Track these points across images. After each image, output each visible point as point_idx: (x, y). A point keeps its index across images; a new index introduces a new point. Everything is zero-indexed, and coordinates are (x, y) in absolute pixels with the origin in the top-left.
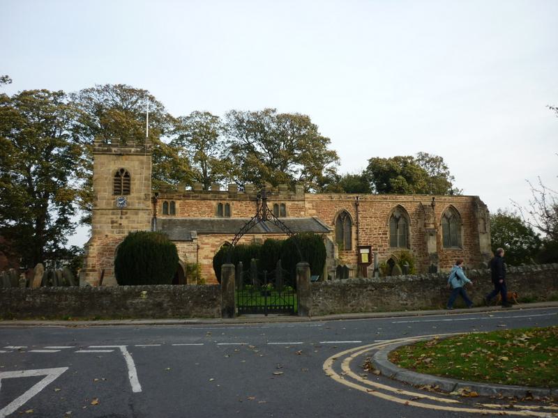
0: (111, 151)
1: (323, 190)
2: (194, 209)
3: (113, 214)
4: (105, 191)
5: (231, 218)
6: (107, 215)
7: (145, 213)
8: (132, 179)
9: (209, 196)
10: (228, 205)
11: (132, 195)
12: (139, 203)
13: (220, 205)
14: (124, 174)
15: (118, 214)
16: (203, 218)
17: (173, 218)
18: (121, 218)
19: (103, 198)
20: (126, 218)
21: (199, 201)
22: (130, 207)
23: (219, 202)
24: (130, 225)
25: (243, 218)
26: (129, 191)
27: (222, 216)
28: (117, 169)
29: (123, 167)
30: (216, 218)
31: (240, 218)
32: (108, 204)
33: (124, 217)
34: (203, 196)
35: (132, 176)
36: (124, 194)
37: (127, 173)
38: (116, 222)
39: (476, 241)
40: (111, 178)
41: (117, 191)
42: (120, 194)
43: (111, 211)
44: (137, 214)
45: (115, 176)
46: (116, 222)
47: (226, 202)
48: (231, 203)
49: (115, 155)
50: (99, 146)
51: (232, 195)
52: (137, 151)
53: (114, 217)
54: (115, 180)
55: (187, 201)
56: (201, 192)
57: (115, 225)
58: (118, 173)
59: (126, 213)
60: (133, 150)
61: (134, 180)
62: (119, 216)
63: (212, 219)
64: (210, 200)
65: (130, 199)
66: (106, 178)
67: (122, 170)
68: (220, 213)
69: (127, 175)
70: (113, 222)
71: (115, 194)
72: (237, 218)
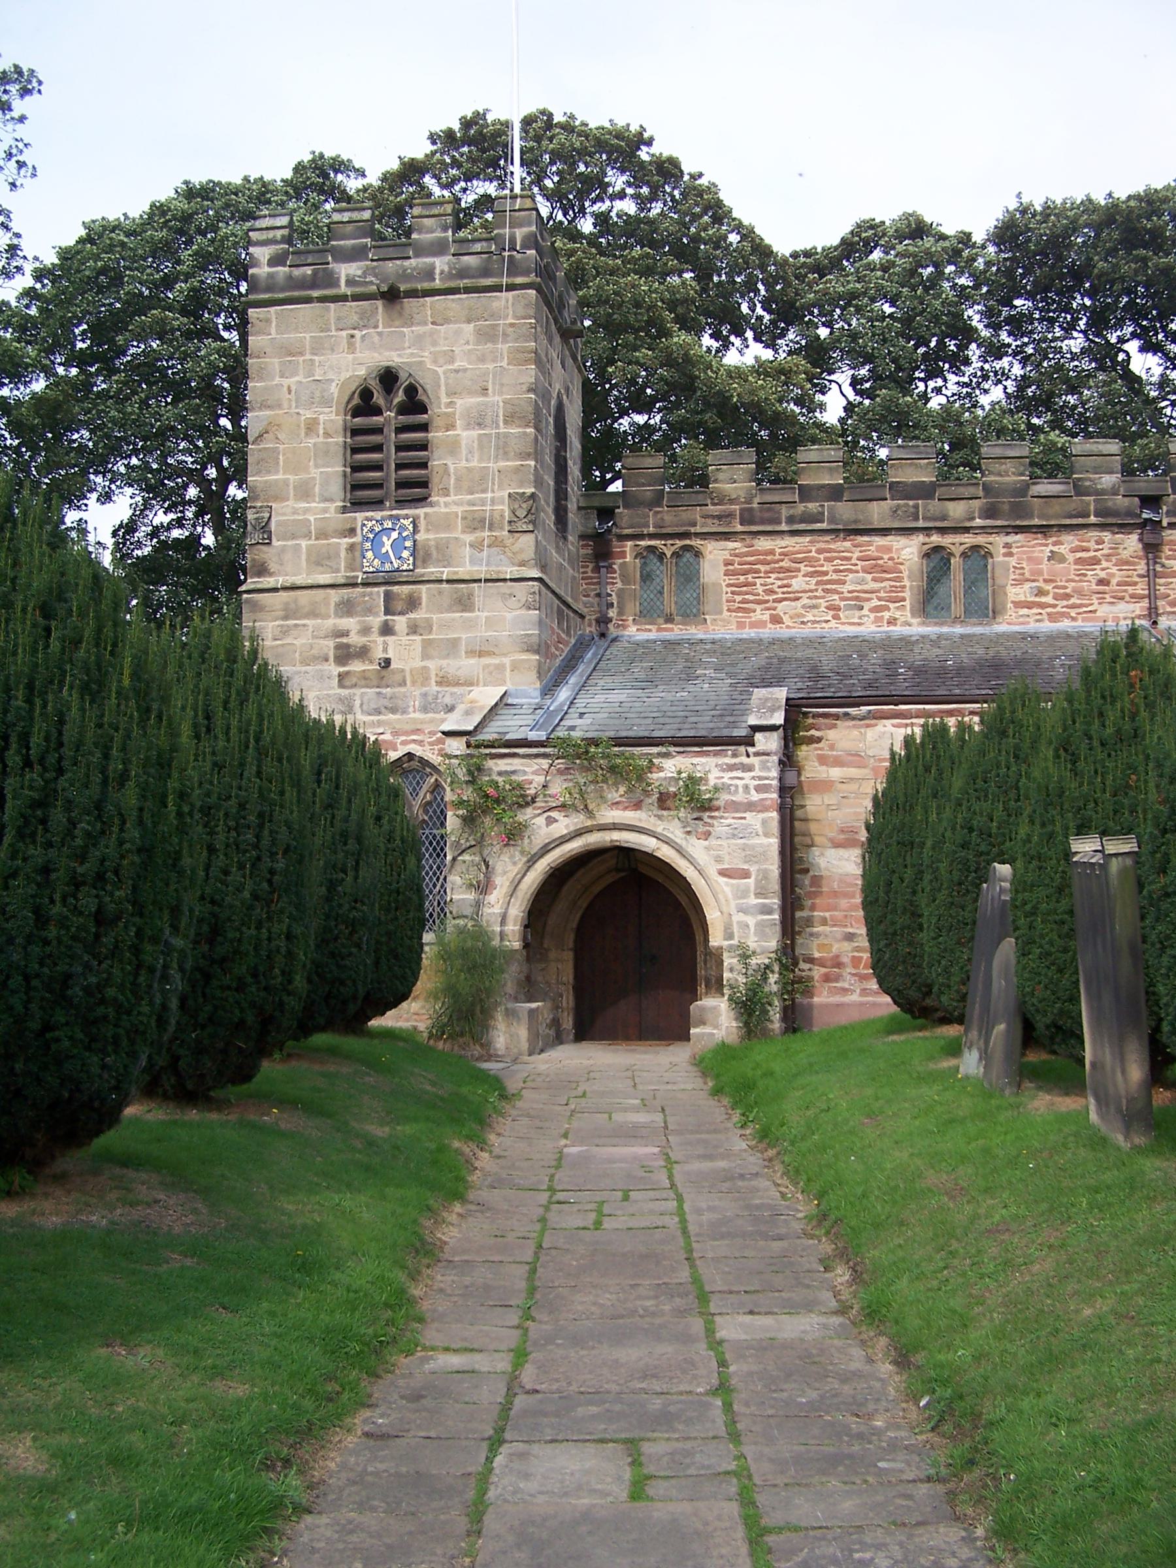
0: (330, 280)
1: (201, 1509)
2: (798, 583)
3: (346, 607)
4: (304, 492)
5: (1001, 627)
6: (313, 614)
7: (505, 597)
8: (437, 422)
9: (878, 512)
10: (978, 555)
11: (446, 504)
12: (477, 546)
13: (937, 559)
14: (400, 397)
15: (369, 611)
16: (851, 630)
17: (695, 632)
18: (387, 630)
19: (298, 531)
20: (413, 629)
21: (823, 542)
22: (431, 571)
23: (936, 539)
24: (431, 665)
25: (1065, 625)
26: (424, 484)
27: (426, 514)
28: (362, 372)
29: (393, 358)
30: (917, 628)
31: (1047, 626)
32: (319, 560)
33: (400, 622)
34: (845, 510)
35: (440, 404)
36: (401, 503)
37: (411, 390)
38: (363, 653)
39: (799, 641)
40: (332, 418)
41: (362, 492)
42: (378, 504)
43: (334, 596)
44: (465, 604)
45: (357, 412)
46: (363, 653)
47: (969, 540)
48: (998, 541)
49: (356, 298)
50: (275, 261)
51: (1005, 501)
52: (463, 273)
53: (350, 623)
54: (355, 432)
55: (763, 544)
56: (835, 493)
57: (356, 666)
58: (366, 394)
59: (413, 603)
60: (440, 264)
61: (451, 426)
62: (377, 620)
63: (898, 630)
64: (884, 532)
65: (433, 526)
66: (311, 427)
67: (388, 378)
68: (929, 601)
69: (414, 404)
70: (345, 654)
71: (357, 505)
72: (1032, 627)
